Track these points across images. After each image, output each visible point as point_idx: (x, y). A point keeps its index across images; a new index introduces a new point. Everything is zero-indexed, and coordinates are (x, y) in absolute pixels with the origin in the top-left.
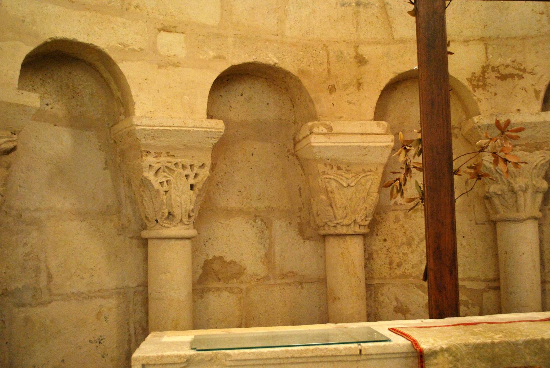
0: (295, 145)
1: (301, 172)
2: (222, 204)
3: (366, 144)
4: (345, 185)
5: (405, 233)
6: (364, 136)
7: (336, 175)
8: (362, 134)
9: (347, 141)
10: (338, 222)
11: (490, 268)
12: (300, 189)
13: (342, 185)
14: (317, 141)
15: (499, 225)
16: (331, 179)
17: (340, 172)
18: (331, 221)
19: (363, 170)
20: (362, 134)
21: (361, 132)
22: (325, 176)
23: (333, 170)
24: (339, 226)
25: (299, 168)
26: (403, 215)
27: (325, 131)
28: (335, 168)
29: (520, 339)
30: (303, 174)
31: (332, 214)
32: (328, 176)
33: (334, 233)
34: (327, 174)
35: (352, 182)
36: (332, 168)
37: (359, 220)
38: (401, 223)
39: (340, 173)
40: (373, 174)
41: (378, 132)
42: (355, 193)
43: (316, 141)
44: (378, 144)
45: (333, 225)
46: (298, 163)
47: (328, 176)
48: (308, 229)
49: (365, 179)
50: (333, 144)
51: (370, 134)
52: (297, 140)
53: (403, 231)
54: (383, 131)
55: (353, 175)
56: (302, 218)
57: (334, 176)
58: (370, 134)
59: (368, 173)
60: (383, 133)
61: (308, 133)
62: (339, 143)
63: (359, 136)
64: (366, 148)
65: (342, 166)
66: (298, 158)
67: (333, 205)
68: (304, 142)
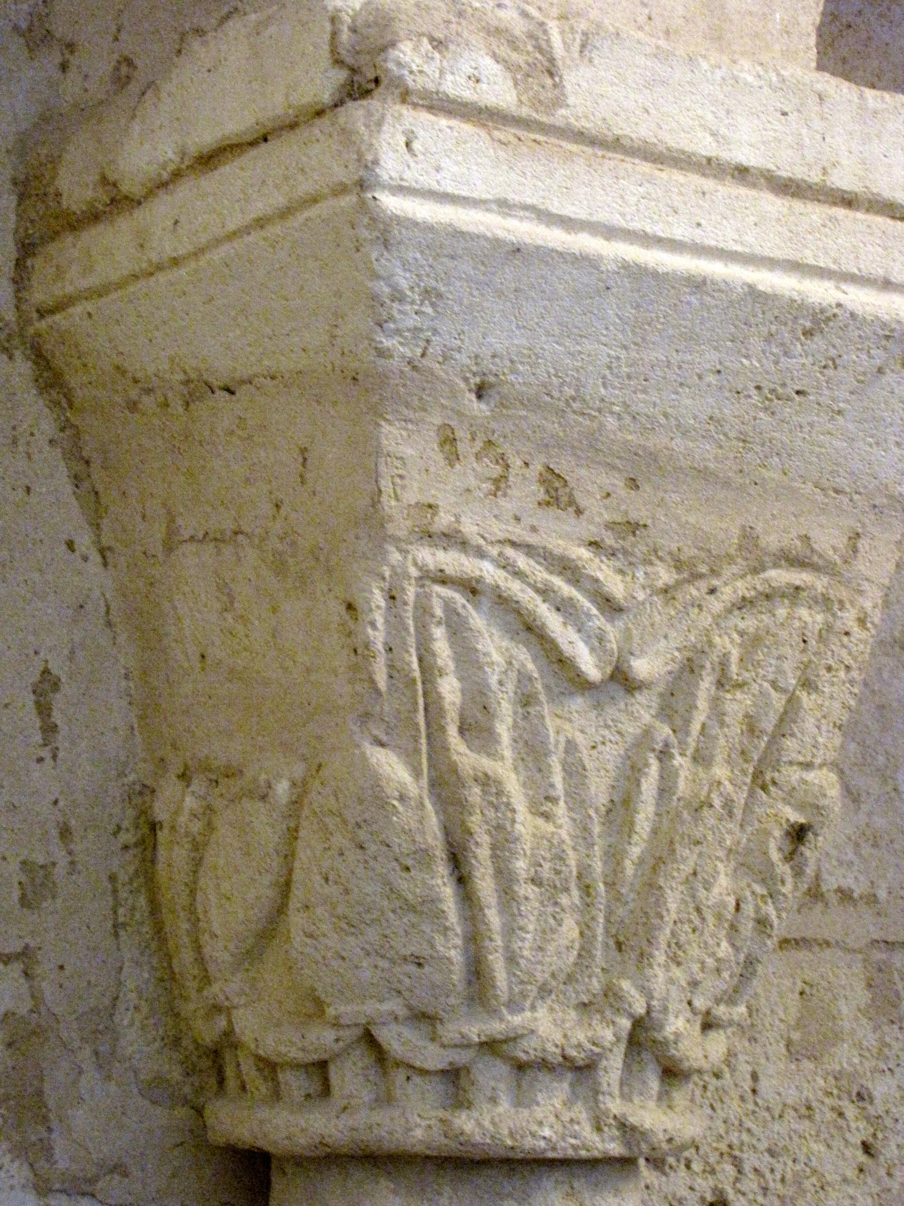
0: (27, 249)
1: (70, 517)
3: (820, 292)
4: (590, 666)
5: (866, 1148)
6: (815, 213)
7: (522, 562)
8: (789, 188)
9: (680, 231)
10: (496, 1028)
12: (46, 686)
13: (559, 662)
14: (429, 181)
15: (332, 1068)
16: (472, 588)
17: (563, 536)
18: (424, 1018)
19: (749, 538)
20: (789, 188)
21: (788, 166)
23: (507, 505)
24: (491, 1075)
25: (54, 476)
26: (863, 996)
27: (499, 91)
28: (525, 491)
30: (85, 541)
31: (453, 952)
32: (450, 560)
33: (440, 1143)
34: (453, 539)
36: (499, 484)
38: (844, 1056)
39: (558, 545)
43: (416, 175)
45: (433, 1057)
46: (48, 427)
47: (450, 560)
48: (90, 1078)
50: (555, 238)
51: (848, 201)
52: (75, 188)
53: (859, 1131)
56: (45, 968)
57: (506, 565)
58: (848, 201)
59: (780, 576)
61: (324, 83)
62: (610, 232)
63: (773, 204)
64: (818, 322)
65: (589, 482)
66: (50, 379)
68: (110, 248)
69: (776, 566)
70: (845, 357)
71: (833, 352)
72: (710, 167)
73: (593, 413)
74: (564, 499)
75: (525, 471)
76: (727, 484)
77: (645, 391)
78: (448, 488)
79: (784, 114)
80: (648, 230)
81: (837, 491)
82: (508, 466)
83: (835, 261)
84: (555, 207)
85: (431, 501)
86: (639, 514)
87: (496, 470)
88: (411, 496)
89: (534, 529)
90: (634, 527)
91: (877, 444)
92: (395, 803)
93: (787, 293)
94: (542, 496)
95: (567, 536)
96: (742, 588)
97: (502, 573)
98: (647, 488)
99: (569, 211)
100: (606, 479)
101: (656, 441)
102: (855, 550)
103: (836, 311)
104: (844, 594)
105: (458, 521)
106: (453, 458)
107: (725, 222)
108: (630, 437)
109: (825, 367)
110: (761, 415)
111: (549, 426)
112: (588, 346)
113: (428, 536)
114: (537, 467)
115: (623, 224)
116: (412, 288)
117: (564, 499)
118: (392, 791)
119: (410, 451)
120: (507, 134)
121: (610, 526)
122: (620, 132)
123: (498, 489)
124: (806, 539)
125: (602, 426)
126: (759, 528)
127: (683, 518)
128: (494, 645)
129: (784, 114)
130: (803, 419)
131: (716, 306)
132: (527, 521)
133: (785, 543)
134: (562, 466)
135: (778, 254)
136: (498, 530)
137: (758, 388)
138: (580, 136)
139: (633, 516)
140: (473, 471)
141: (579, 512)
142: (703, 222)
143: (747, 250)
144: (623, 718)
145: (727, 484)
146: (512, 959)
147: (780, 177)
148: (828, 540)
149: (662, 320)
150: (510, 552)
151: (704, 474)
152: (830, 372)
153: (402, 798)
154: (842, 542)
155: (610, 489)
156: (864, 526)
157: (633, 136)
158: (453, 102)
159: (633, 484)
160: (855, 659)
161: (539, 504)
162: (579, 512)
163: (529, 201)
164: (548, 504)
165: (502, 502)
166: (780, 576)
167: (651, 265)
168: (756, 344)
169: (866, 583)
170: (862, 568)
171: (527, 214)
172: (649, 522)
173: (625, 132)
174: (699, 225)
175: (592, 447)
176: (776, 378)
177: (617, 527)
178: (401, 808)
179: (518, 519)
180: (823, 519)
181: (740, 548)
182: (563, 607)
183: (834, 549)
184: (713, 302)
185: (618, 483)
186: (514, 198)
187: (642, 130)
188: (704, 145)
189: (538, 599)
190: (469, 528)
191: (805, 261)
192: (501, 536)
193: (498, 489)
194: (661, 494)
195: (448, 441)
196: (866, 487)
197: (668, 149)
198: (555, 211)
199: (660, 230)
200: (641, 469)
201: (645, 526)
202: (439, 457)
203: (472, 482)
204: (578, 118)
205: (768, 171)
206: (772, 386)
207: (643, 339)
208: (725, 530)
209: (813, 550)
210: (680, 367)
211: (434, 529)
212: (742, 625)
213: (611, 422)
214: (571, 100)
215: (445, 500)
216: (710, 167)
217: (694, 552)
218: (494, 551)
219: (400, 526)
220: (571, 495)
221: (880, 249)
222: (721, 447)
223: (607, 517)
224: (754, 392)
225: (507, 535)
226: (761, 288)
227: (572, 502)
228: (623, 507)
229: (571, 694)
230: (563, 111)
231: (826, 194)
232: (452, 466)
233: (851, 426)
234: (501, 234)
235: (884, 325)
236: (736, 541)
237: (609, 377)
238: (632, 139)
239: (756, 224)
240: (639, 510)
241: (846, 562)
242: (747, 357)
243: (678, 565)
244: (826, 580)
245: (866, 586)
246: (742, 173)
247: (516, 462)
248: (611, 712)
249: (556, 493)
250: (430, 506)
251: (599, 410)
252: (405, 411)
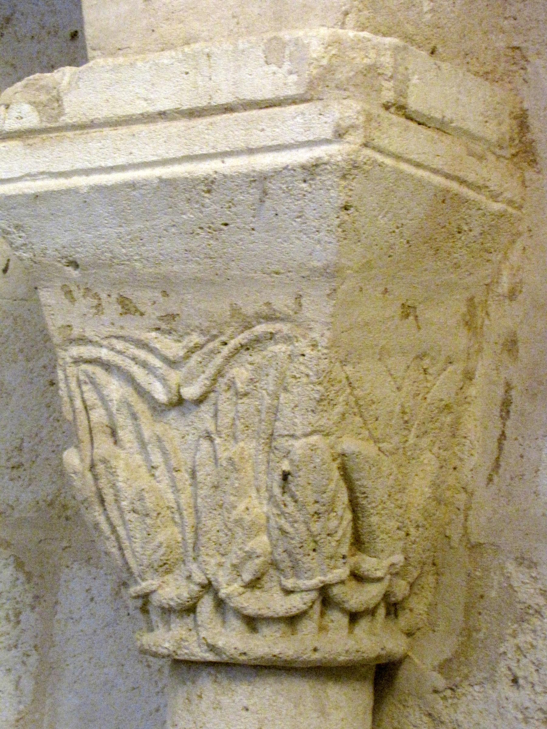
2: (328, 691)
4: (160, 394)
6: (201, 123)
7: (120, 345)
8: (193, 114)
9: (121, 160)
11: (382, 649)
17: (134, 328)
19: (235, 311)
20: (193, 114)
22: (75, 351)
28: (112, 310)
29: (159, 652)
34: (82, 340)
35: (189, 379)
37: (229, 588)
40: (284, 328)
41: (267, 93)
42: (209, 437)
44: (265, 162)
49: (257, 358)
51: (228, 109)
54: (292, 86)
55: (195, 338)
58: (228, 109)
59: (261, 329)
60: (291, 91)
65: (143, 297)
67: (109, 498)
69: (259, 323)
70: (236, 199)
71: (228, 198)
72: (147, 118)
73: (127, 263)
74: (133, 309)
75: (109, 299)
76: (213, 283)
77: (144, 245)
78: (75, 315)
79: (187, 73)
80: (103, 165)
81: (277, 273)
82: (100, 299)
83: (214, 148)
84: (55, 169)
85: (68, 324)
86: (174, 309)
87: (96, 302)
88: (60, 322)
89: (122, 328)
90: (173, 317)
91: (285, 241)
92: (73, 475)
93: (182, 175)
94: (120, 310)
95: (137, 328)
96: (242, 338)
97: (112, 353)
98: (172, 294)
99: (63, 168)
100: (148, 294)
101: (164, 269)
102: (300, 305)
103: (215, 176)
104: (298, 332)
105: (84, 331)
106: (73, 300)
107: (147, 147)
108: (151, 270)
109: (230, 208)
110: (211, 242)
111: (111, 275)
112: (104, 231)
113: (72, 341)
114: (114, 296)
115: (90, 166)
116: (9, 227)
117: (133, 309)
118: (69, 470)
119: (53, 302)
120: (36, 140)
121: (161, 318)
122: (93, 117)
123: (99, 311)
124: (268, 304)
125: (134, 268)
126: (240, 303)
127: (196, 306)
128: (115, 388)
129: (187, 73)
130: (235, 238)
131: (149, 193)
132: (118, 324)
133: (257, 308)
134: (127, 292)
135: (180, 154)
136: (106, 331)
137: (201, 228)
138: (74, 127)
139: (170, 311)
140: (84, 304)
141: (142, 314)
142: (133, 151)
143: (160, 158)
144: (196, 420)
145: (213, 283)
146: (133, 552)
147: (183, 110)
148: (282, 302)
149: (129, 208)
150: (114, 341)
151: (197, 280)
152: (233, 209)
153: (75, 473)
154: (291, 302)
155: (155, 299)
156: (302, 289)
157: (99, 117)
158: (11, 133)
159: (165, 294)
160: (311, 369)
161: (121, 314)
162: (142, 314)
163: (41, 170)
164: (126, 313)
165: (102, 317)
166: (261, 329)
167: (104, 183)
168: (183, 205)
169: (312, 323)
170: (308, 314)
171: (45, 176)
172: (179, 312)
173: (96, 117)
174: (131, 153)
175: (136, 280)
176: (206, 220)
177: (165, 318)
178: (75, 478)
179: (113, 324)
180: (275, 291)
181: (232, 316)
182: (144, 365)
183: (286, 306)
184: (146, 192)
185: (158, 294)
186: (34, 171)
187: (104, 112)
188: (141, 107)
189: (132, 363)
190: (89, 334)
191: (195, 153)
192: (107, 334)
193: (99, 311)
194: (181, 297)
195: (68, 293)
196: (292, 268)
197: (119, 117)
198: (54, 171)
199: (110, 163)
200: (166, 285)
201: (178, 315)
202: (66, 301)
203: (86, 310)
204: (71, 118)
205: (176, 109)
206: (207, 225)
207: (126, 220)
208: (221, 308)
209: (274, 310)
210: (153, 228)
211: (72, 337)
212: (250, 359)
213: (138, 265)
214: (67, 110)
215: (76, 322)
216: (147, 118)
217: (207, 324)
218: (105, 343)
219: (57, 339)
220: (135, 307)
221: (242, 131)
222: (199, 264)
223: (158, 314)
224: (199, 231)
225: (109, 333)
226: (164, 177)
227: (137, 310)
228: (163, 307)
229: (169, 410)
230: (63, 118)
231: (214, 110)
232: (74, 305)
233: (263, 235)
234: (27, 191)
235: (247, 175)
236: (229, 313)
237: (122, 243)
238: (99, 119)
239: (165, 142)
240: (171, 307)
241: (296, 313)
242: (184, 214)
243: (202, 332)
244: (289, 325)
245: (313, 325)
246: (163, 115)
247: (103, 296)
248: (191, 417)
249: (127, 307)
250: (69, 326)
251: (128, 260)
252: (45, 283)
